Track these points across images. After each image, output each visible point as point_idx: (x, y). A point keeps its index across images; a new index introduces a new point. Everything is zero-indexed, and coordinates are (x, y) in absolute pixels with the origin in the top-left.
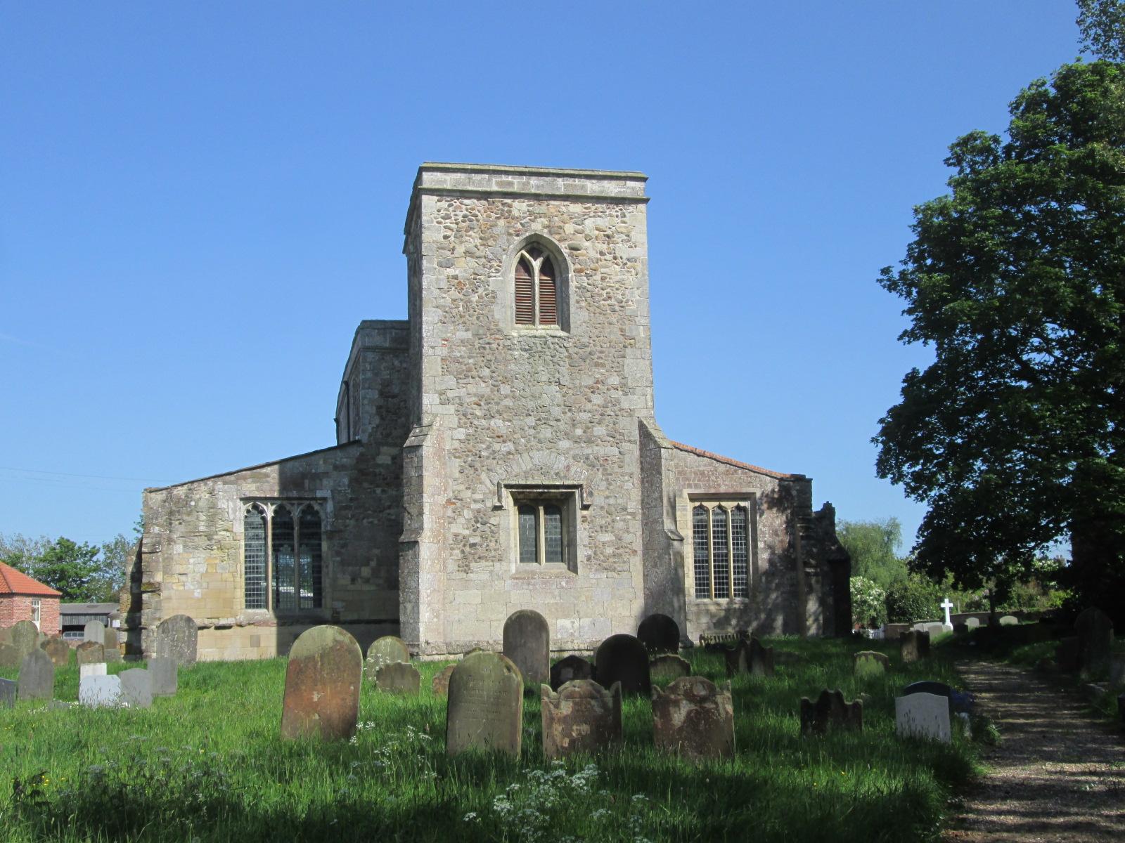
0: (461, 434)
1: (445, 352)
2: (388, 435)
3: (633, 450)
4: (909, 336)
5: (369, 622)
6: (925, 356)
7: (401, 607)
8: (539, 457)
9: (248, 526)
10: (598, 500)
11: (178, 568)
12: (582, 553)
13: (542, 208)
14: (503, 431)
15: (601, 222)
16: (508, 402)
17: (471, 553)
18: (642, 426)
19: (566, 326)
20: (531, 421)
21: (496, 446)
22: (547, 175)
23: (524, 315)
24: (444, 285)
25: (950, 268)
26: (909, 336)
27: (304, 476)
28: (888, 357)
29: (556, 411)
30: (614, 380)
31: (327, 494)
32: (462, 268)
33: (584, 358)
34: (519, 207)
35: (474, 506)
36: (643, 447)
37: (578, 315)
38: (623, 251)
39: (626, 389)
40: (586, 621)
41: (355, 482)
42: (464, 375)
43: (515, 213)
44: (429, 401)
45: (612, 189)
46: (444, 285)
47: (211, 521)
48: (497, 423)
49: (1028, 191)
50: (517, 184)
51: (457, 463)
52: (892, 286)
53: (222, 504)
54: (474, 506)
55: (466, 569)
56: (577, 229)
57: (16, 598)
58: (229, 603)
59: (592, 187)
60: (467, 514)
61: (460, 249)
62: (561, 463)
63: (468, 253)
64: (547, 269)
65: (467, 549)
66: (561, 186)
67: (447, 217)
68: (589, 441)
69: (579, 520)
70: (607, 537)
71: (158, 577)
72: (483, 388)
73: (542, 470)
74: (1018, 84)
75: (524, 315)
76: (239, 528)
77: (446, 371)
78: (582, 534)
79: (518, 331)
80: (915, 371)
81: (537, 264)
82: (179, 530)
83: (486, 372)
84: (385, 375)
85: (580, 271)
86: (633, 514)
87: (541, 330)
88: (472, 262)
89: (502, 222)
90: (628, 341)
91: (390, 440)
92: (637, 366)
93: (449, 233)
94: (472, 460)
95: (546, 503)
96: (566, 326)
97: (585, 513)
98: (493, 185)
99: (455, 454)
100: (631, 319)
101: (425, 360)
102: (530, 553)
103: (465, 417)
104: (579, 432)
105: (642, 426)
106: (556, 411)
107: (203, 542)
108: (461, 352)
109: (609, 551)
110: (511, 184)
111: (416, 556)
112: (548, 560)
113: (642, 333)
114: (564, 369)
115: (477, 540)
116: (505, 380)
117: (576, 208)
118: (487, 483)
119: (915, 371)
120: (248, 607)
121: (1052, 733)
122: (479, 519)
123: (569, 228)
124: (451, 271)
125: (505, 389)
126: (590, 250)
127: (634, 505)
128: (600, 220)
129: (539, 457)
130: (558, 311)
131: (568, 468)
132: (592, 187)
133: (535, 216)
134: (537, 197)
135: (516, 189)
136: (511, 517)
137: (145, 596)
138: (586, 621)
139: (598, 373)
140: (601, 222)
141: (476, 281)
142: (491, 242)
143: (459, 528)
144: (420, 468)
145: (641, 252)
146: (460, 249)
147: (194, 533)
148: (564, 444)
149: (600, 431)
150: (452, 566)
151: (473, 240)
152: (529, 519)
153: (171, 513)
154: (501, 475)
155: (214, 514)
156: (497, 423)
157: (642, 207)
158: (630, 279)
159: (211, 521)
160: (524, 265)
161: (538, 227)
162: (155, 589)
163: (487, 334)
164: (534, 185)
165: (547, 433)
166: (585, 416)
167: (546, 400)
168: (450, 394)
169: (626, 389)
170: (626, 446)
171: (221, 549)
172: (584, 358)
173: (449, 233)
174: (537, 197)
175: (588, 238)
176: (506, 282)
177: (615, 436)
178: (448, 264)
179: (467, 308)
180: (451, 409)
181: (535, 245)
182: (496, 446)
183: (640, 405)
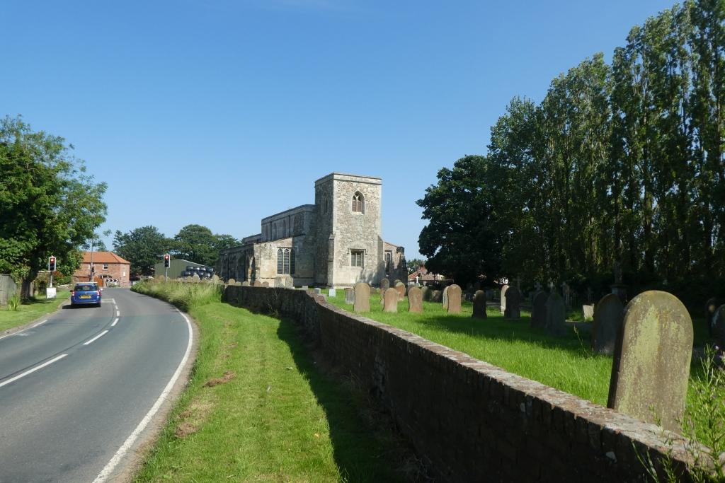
0: (341, 237)
3: (376, 242)
4: (423, 218)
8: (357, 242)
10: (368, 253)
12: (365, 265)
13: (359, 185)
15: (372, 189)
17: (342, 264)
18: (379, 237)
19: (363, 213)
23: (354, 210)
26: (423, 218)
29: (361, 233)
32: (342, 198)
33: (367, 221)
34: (355, 184)
37: (366, 211)
41: (303, 244)
44: (334, 229)
45: (374, 181)
48: (349, 235)
49: (551, 203)
50: (354, 179)
51: (340, 243)
55: (341, 267)
56: (367, 190)
57: (121, 265)
59: (370, 180)
61: (342, 194)
63: (344, 195)
64: (359, 199)
66: (363, 180)
70: (370, 261)
71: (259, 266)
73: (358, 245)
74: (456, 159)
75: (354, 210)
76: (276, 254)
77: (338, 222)
78: (365, 260)
79: (353, 213)
80: (425, 227)
81: (357, 198)
82: (263, 254)
84: (311, 218)
87: (358, 213)
90: (377, 217)
94: (343, 244)
95: (357, 253)
96: (363, 213)
98: (349, 179)
100: (377, 212)
102: (353, 264)
105: (379, 237)
108: (341, 218)
111: (332, 264)
113: (379, 215)
117: (367, 185)
119: (425, 227)
120: (278, 273)
121: (27, 326)
122: (344, 256)
123: (365, 190)
125: (351, 227)
126: (369, 195)
127: (376, 254)
128: (371, 188)
130: (361, 209)
132: (370, 180)
134: (358, 182)
135: (354, 180)
136: (350, 256)
139: (370, 224)
140: (372, 189)
145: (380, 196)
146: (342, 194)
148: (362, 240)
149: (370, 237)
152: (354, 256)
154: (349, 246)
160: (354, 198)
161: (358, 189)
162: (258, 269)
163: (347, 213)
164: (358, 179)
165: (359, 237)
172: (367, 221)
174: (358, 182)
176: (350, 202)
177: (373, 239)
178: (339, 197)
181: (357, 194)
183: (378, 232)
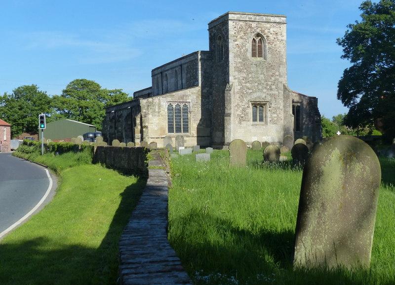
1: (235, 65)
2: (206, 84)
5: (201, 137)
6: (348, 64)
7: (225, 133)
8: (258, 94)
9: (168, 110)
10: (273, 105)
11: (150, 122)
12: (269, 119)
14: (250, 87)
15: (275, 29)
16: (251, 79)
17: (242, 119)
18: (284, 86)
20: (256, 84)
21: (248, 91)
22: (261, 15)
24: (235, 47)
25: (353, 41)
27: (184, 96)
28: (340, 65)
30: (277, 73)
31: (190, 101)
32: (239, 42)
35: (243, 107)
36: (284, 91)
37: (269, 56)
38: (280, 37)
39: (280, 76)
40: (270, 137)
42: (240, 71)
43: (253, 26)
44: (231, 78)
46: (235, 47)
47: (159, 108)
48: (248, 85)
52: (340, 44)
53: (162, 103)
54: (243, 107)
55: (240, 123)
56: (270, 31)
58: (164, 131)
60: (241, 109)
61: (239, 37)
62: (263, 96)
65: (241, 118)
67: (235, 27)
68: (271, 90)
69: (268, 111)
70: (275, 115)
71: (147, 124)
72: (245, 75)
75: (254, 55)
82: (150, 111)
83: (245, 71)
85: (269, 43)
86: (281, 109)
87: (259, 59)
88: (242, 40)
89: (249, 29)
91: (207, 86)
92: (283, 70)
93: (236, 32)
96: (265, 58)
97: (270, 109)
99: (238, 93)
101: (230, 68)
103: (240, 83)
104: (268, 87)
105: (284, 86)
106: (263, 82)
107: (157, 114)
108: (239, 65)
109: (275, 119)
110: (251, 18)
112: (260, 121)
114: (265, 70)
115: (243, 116)
116: (250, 73)
118: (246, 100)
122: (244, 110)
123: (266, 31)
124: (236, 43)
125: (250, 75)
126: (272, 37)
129: (258, 94)
131: (265, 97)
132: (272, 19)
133: (258, 27)
137: (144, 129)
138: (270, 137)
140: (275, 29)
141: (243, 46)
142: (247, 35)
143: (239, 113)
144: (230, 97)
145: (285, 38)
146: (239, 37)
147: (154, 111)
148: (265, 90)
150: (237, 122)
151: (242, 34)
153: (148, 106)
154: (249, 98)
155: (160, 106)
156: (248, 85)
157: (285, 25)
158: (282, 46)
159: (159, 108)
161: (258, 31)
162: (146, 127)
163: (245, 59)
166: (270, 83)
167: (260, 79)
168: (236, 77)
169: (280, 76)
170: (280, 91)
171: (162, 116)
172: (270, 67)
173: (236, 32)
175: (271, 34)
176: (249, 46)
178: (235, 41)
179: (240, 53)
180: (237, 80)
182: (248, 91)
183: (284, 80)
